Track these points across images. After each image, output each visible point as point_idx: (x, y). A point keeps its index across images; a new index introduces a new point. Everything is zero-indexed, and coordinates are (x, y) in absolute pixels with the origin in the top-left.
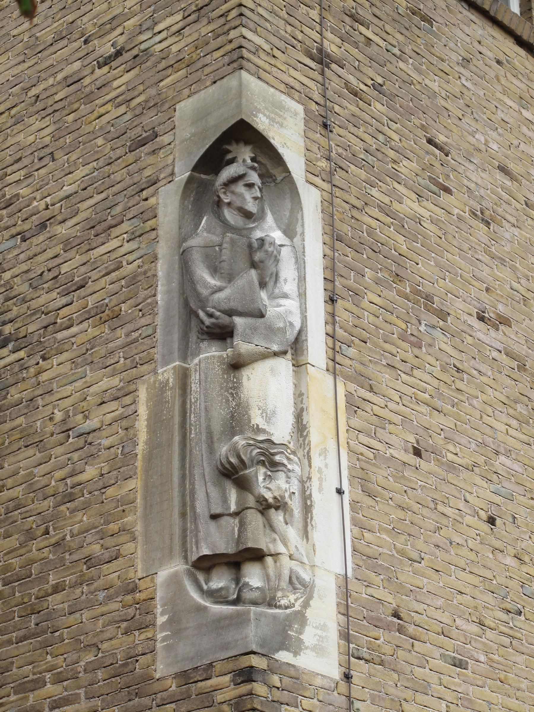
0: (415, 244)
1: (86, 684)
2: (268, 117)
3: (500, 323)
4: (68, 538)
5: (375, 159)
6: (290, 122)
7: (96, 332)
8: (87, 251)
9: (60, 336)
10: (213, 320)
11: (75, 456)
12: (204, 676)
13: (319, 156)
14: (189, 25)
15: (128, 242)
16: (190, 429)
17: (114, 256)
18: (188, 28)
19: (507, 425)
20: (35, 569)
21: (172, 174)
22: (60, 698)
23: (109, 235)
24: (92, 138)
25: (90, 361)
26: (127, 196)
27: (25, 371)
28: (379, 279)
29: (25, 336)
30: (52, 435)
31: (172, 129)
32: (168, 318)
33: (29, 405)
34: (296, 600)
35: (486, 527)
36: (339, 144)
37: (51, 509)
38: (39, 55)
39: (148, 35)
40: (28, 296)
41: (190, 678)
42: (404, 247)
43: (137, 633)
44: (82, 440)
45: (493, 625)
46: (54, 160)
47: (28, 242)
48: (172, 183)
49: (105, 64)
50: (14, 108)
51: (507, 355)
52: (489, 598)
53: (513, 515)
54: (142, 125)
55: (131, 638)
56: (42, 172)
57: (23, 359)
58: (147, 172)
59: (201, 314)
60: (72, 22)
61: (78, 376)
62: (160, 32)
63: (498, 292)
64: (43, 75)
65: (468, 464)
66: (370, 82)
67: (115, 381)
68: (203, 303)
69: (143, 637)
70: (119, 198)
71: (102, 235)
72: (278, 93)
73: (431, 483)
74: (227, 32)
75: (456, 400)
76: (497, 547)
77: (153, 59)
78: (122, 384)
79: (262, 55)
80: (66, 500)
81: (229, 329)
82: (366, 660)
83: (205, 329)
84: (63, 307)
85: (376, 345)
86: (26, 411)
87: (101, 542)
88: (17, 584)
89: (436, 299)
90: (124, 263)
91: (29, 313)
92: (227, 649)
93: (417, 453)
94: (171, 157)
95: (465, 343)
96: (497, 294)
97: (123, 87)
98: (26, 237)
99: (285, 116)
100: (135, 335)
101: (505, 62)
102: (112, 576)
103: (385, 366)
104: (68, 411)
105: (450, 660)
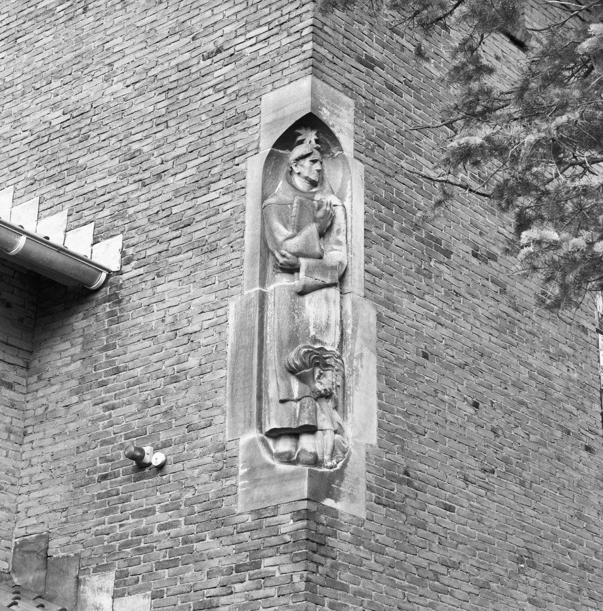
0: (430, 201)
1: (186, 514)
2: (329, 110)
3: (489, 258)
4: (174, 408)
5: (404, 138)
6: (344, 113)
7: (198, 260)
8: (192, 199)
9: (171, 260)
10: (285, 259)
11: (181, 349)
12: (272, 514)
13: (364, 138)
14: (273, 36)
15: (223, 195)
16: (266, 336)
17: (212, 204)
18: (272, 38)
19: (490, 334)
20: (149, 429)
21: (258, 148)
22: (166, 523)
23: (209, 189)
24: (197, 114)
25: (193, 281)
26: (223, 161)
27: (144, 284)
28: (404, 229)
29: (145, 258)
30: (164, 333)
31: (258, 114)
32: (253, 255)
33: (146, 309)
34: (338, 463)
35: (471, 410)
36: (379, 128)
37: (162, 387)
38: (158, 44)
39: (242, 39)
40: (147, 228)
41: (262, 515)
42: (422, 204)
43: (224, 480)
44: (186, 338)
45: (474, 481)
46: (167, 127)
47: (147, 187)
48: (257, 155)
49: (209, 58)
50: (137, 84)
51: (492, 282)
52: (471, 461)
53: (491, 401)
54: (235, 108)
55: (219, 483)
56: (159, 135)
57: (142, 274)
58: (239, 145)
59: (277, 255)
60: (183, 22)
61: (184, 291)
62: (250, 38)
63: (489, 235)
64: (161, 61)
65: (461, 363)
66: (402, 79)
67: (212, 298)
68: (279, 246)
69: (229, 483)
70: (218, 161)
71: (203, 188)
72: (337, 92)
73: (434, 378)
74: (302, 46)
75: (454, 317)
76: (479, 423)
77: (245, 58)
78: (217, 300)
79: (327, 63)
80: (174, 381)
81: (297, 267)
82: (384, 505)
83: (279, 265)
84: (174, 239)
85: (400, 278)
86: (144, 313)
87: (199, 413)
88: (135, 439)
89: (443, 242)
90: (220, 211)
91: (148, 240)
92: (289, 496)
93: (425, 356)
94: (257, 135)
95: (463, 274)
96: (487, 237)
97: (222, 77)
98: (146, 184)
99: (341, 108)
100: (227, 265)
101: (502, 57)
102: (207, 439)
103: (405, 293)
104: (176, 316)
105: (442, 506)
